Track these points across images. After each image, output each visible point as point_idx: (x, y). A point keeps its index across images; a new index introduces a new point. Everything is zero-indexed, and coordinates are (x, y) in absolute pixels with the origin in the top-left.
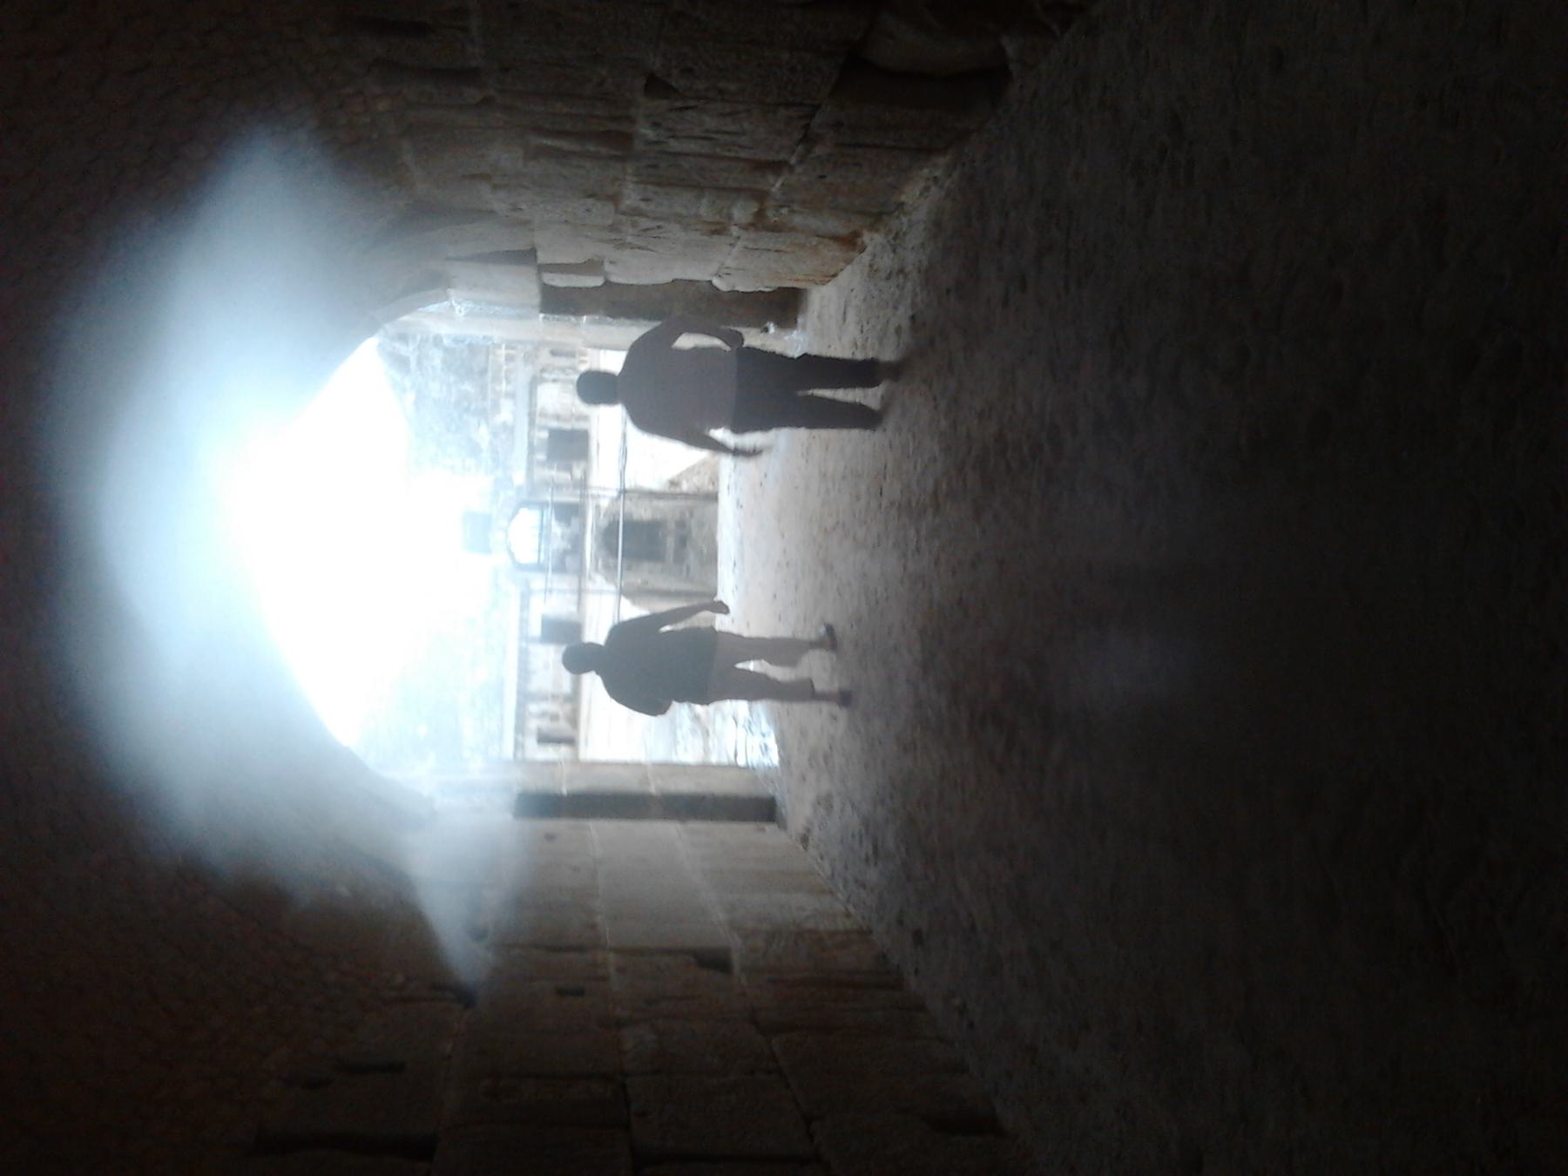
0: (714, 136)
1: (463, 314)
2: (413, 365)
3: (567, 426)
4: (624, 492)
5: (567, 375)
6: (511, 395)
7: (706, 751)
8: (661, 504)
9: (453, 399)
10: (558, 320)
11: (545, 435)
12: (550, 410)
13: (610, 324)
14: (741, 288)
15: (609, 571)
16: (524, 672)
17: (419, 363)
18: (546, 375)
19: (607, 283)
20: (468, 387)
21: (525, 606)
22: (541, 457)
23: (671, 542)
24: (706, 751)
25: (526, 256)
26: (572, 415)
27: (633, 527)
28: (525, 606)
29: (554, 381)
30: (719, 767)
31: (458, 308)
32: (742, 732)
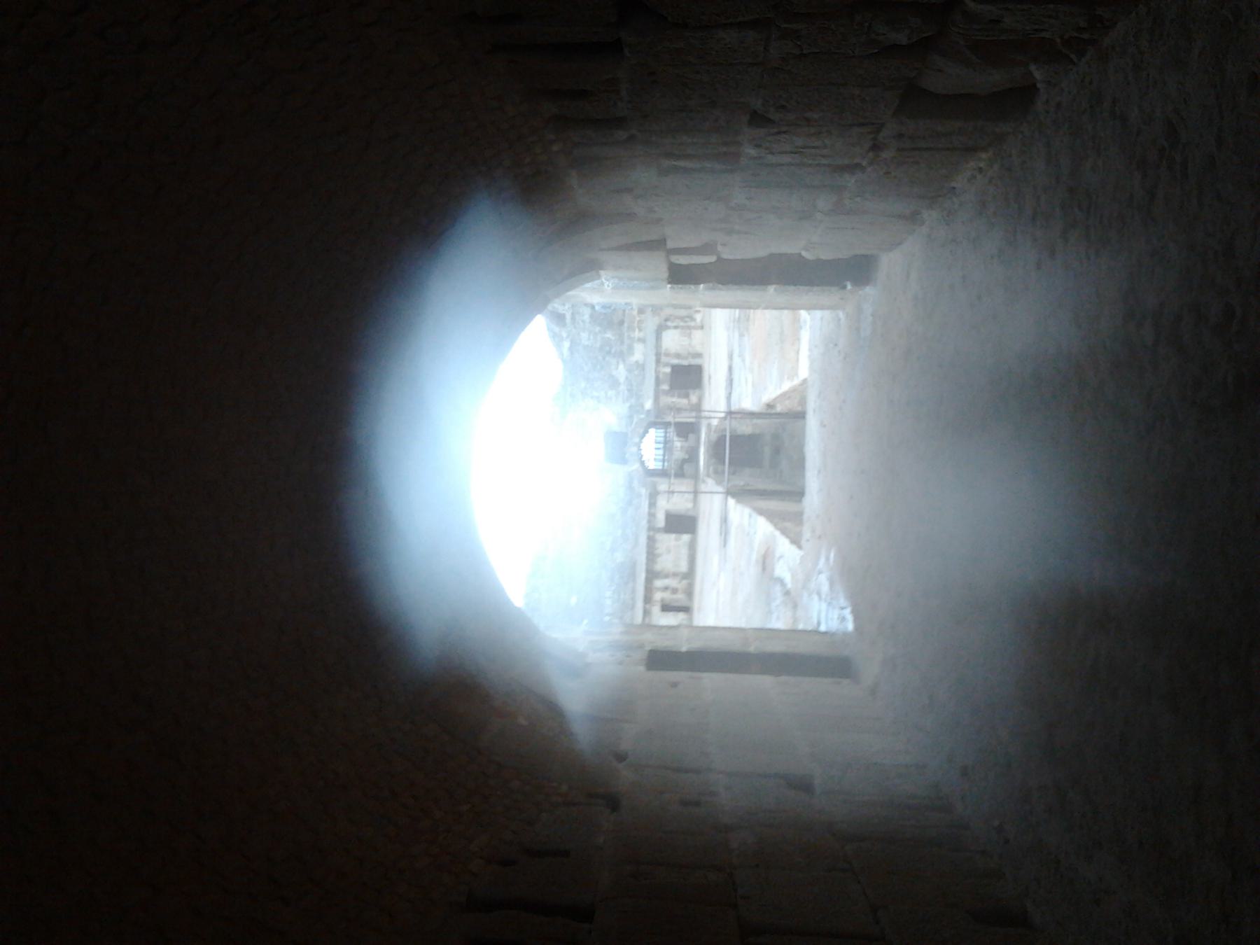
0: (801, 150)
1: (609, 288)
2: (568, 317)
3: (685, 363)
4: (730, 413)
5: (686, 322)
6: (642, 340)
7: (795, 620)
8: (759, 421)
9: (598, 345)
10: (681, 288)
11: (668, 370)
12: (673, 351)
13: (720, 289)
14: (823, 257)
15: (718, 475)
16: (652, 555)
17: (573, 318)
18: (669, 324)
19: (720, 259)
20: (609, 335)
21: (652, 504)
22: (665, 387)
23: (767, 451)
24: (795, 620)
25: (657, 245)
26: (689, 354)
27: (737, 439)
28: (652, 504)
29: (676, 327)
30: (804, 632)
31: (607, 283)
32: (824, 606)
